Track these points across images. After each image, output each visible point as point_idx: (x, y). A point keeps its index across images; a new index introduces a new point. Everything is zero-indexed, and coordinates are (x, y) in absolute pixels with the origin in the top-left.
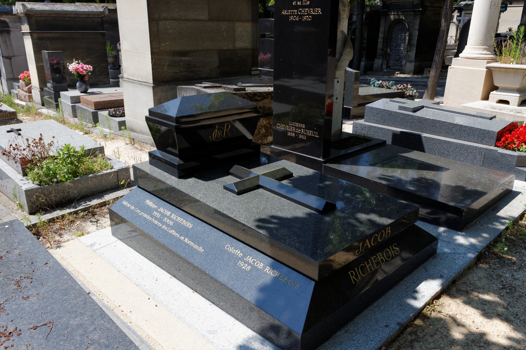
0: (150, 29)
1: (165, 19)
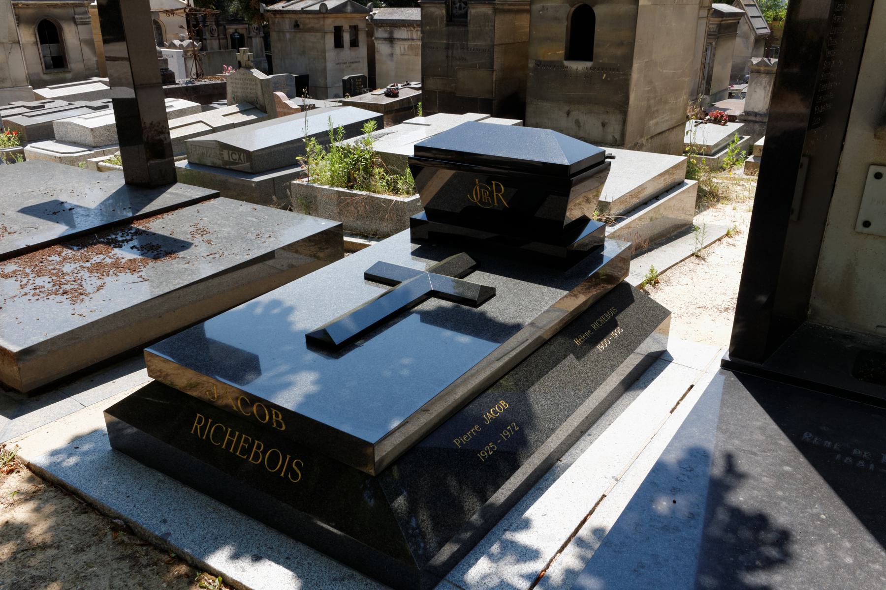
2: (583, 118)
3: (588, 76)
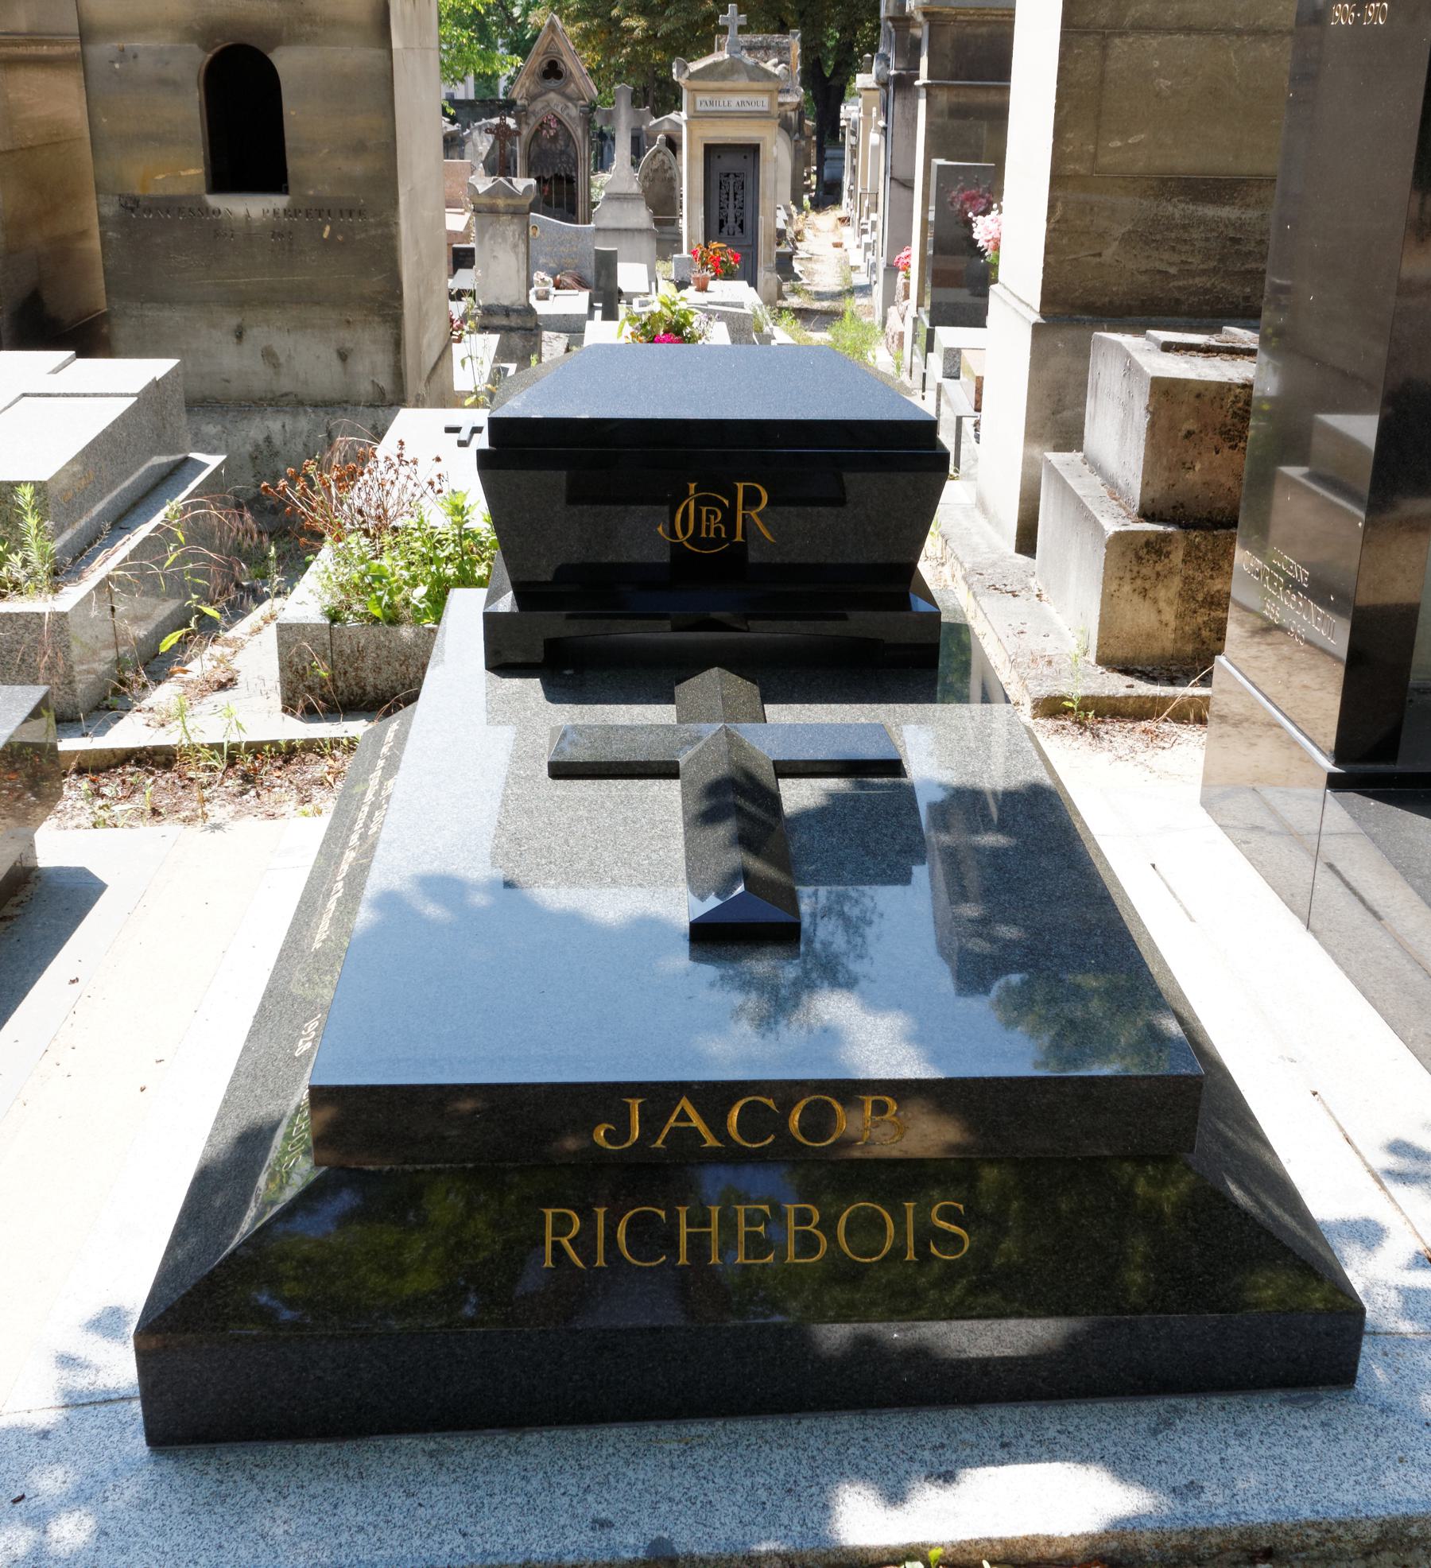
0: (1061, 69)
1: (1143, 27)
2: (282, 343)
3: (280, 234)
